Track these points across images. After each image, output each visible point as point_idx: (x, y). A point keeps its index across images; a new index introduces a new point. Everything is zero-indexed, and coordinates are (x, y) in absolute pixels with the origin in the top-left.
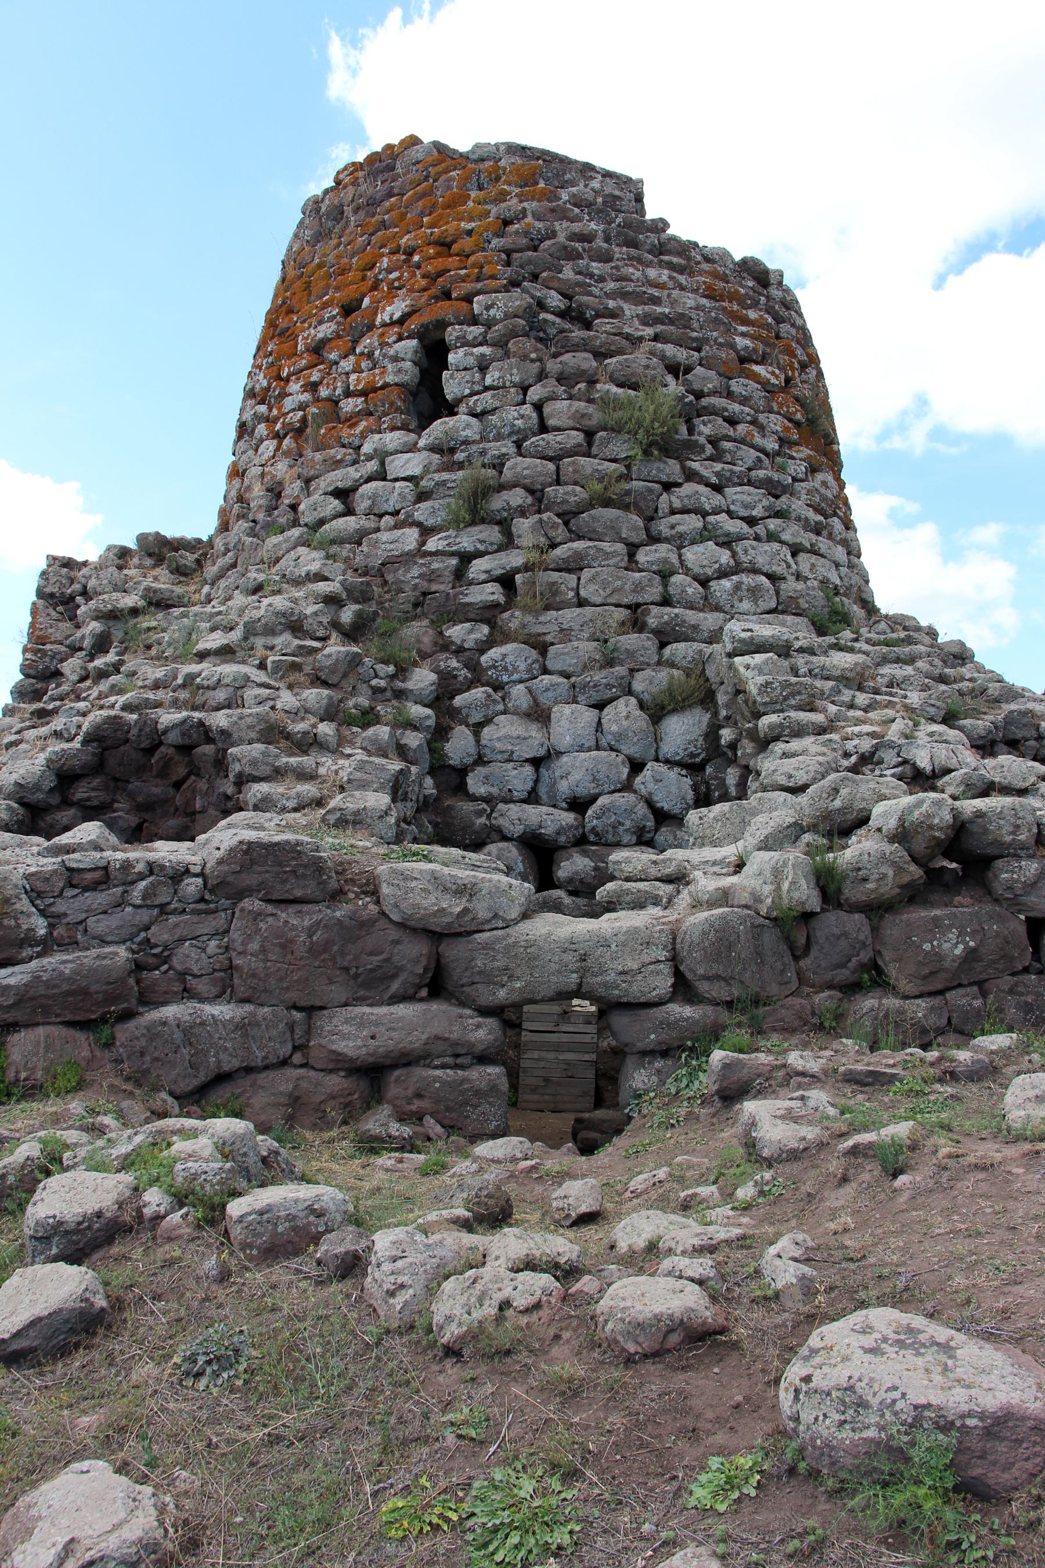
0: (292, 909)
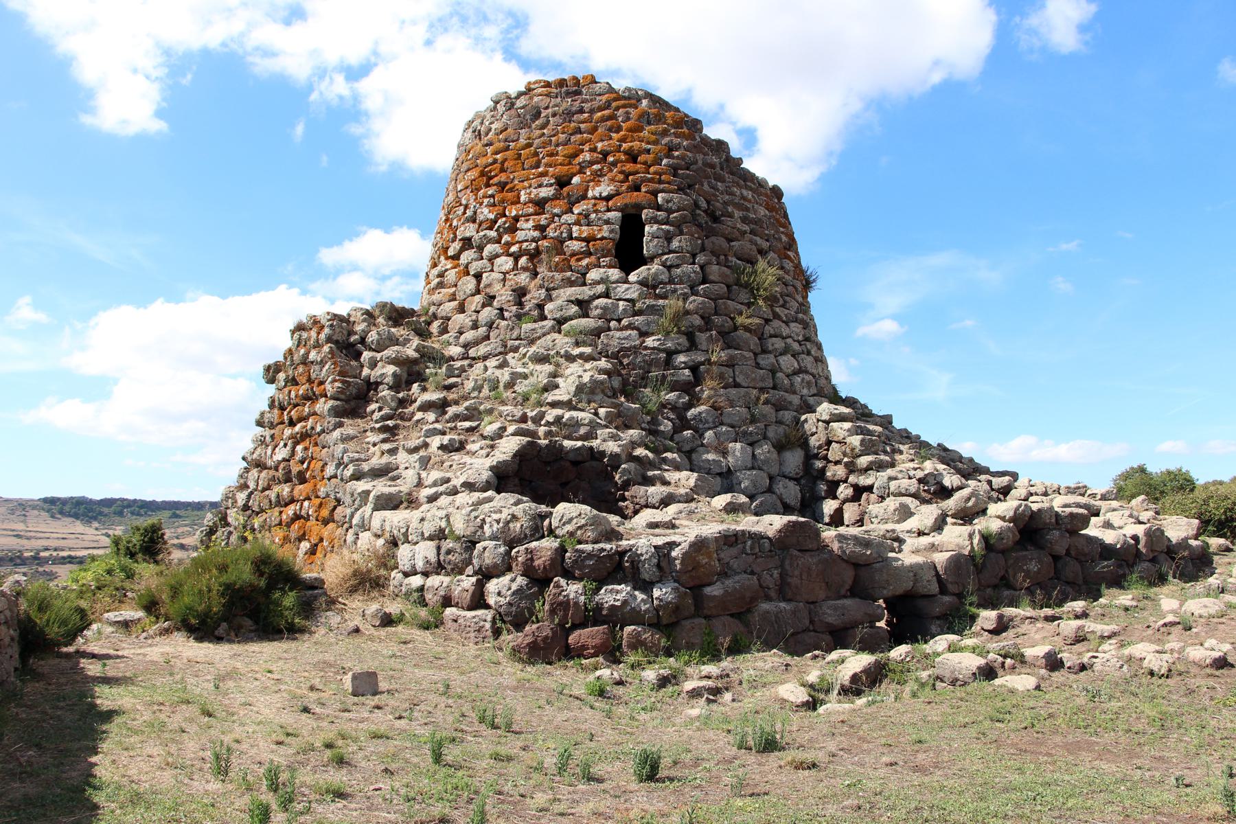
0: (808, 554)
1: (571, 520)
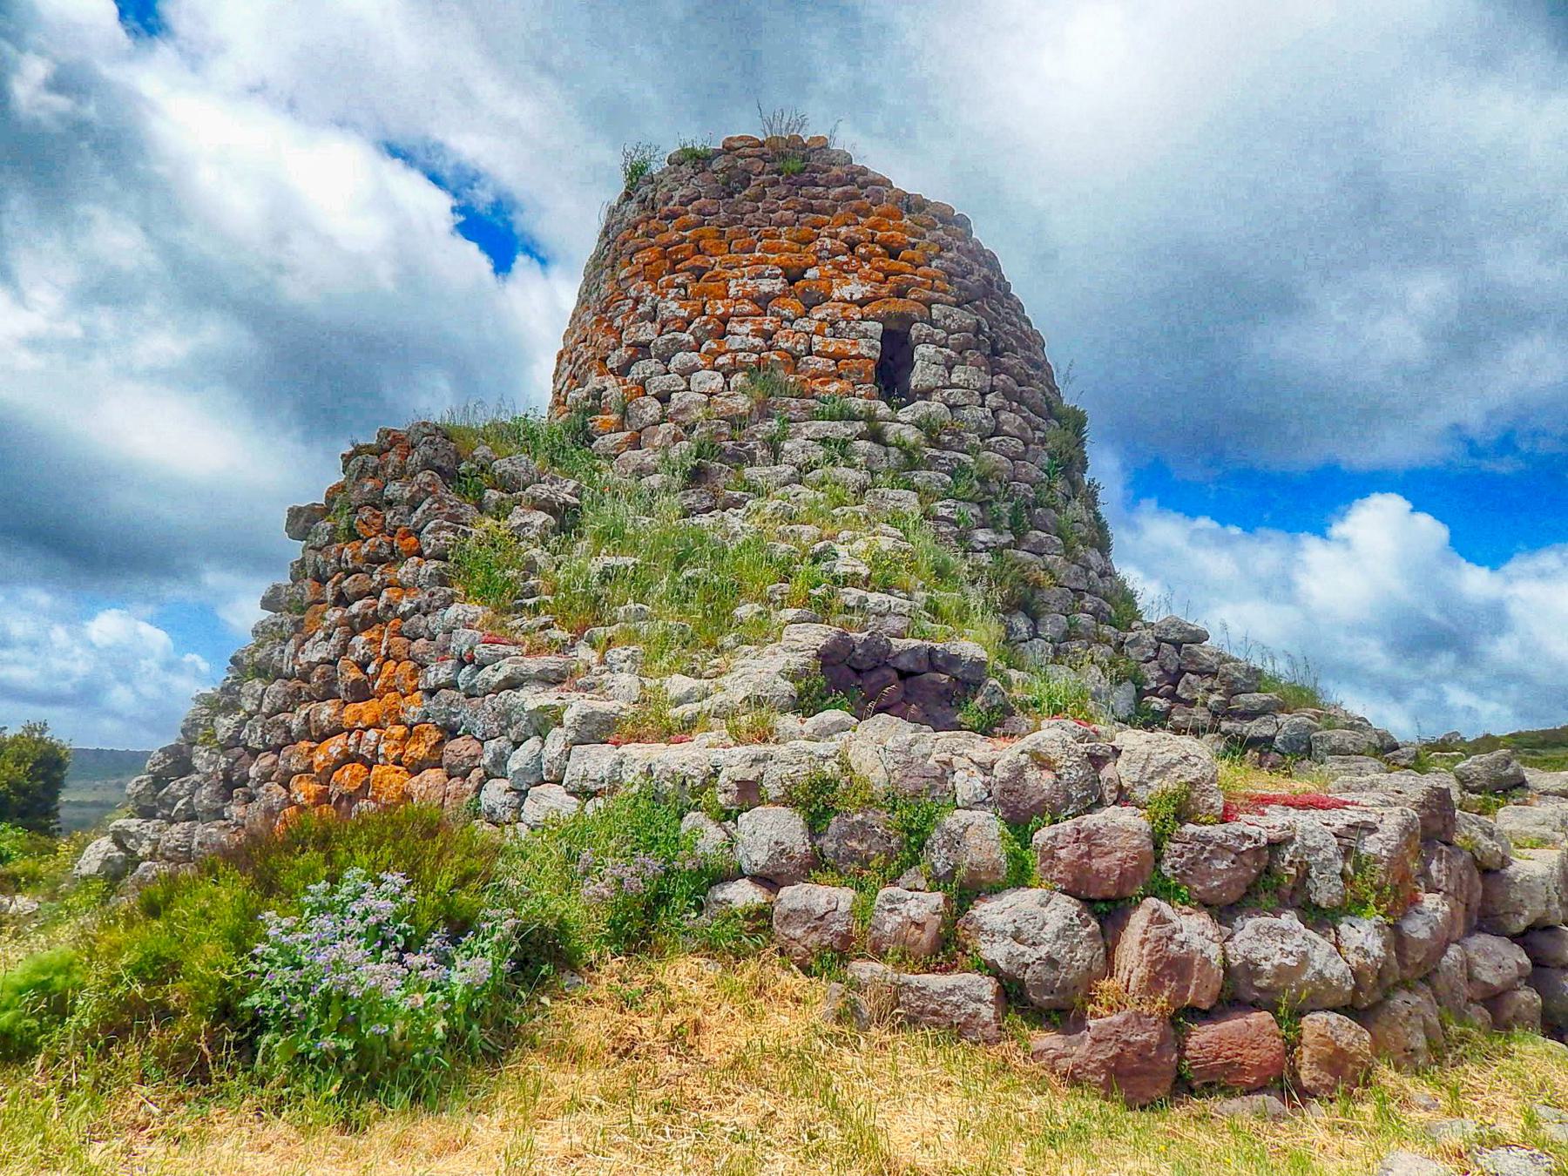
1: (1169, 766)
